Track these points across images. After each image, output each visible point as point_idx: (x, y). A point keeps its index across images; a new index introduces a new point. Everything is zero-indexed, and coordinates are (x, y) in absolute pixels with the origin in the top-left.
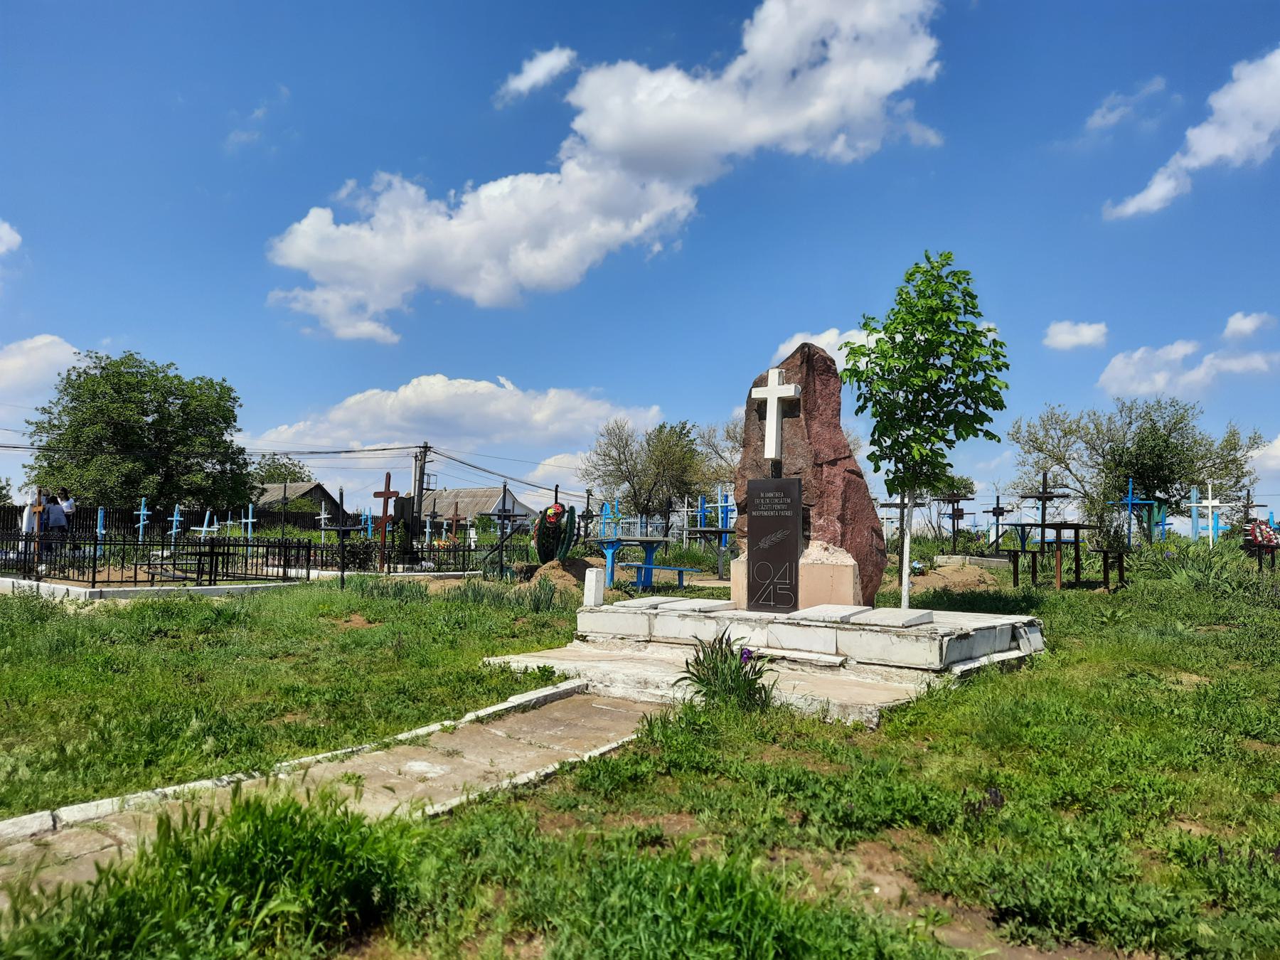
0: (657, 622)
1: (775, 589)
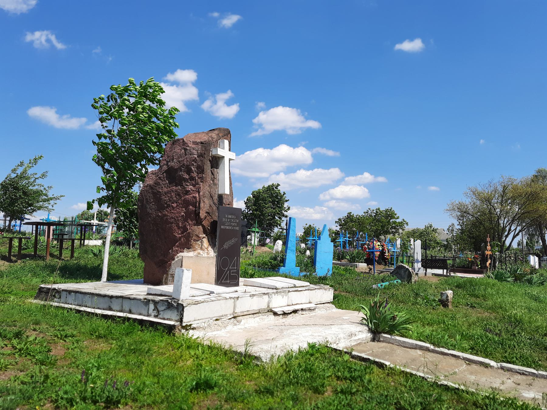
0: (238, 302)
1: (230, 273)
